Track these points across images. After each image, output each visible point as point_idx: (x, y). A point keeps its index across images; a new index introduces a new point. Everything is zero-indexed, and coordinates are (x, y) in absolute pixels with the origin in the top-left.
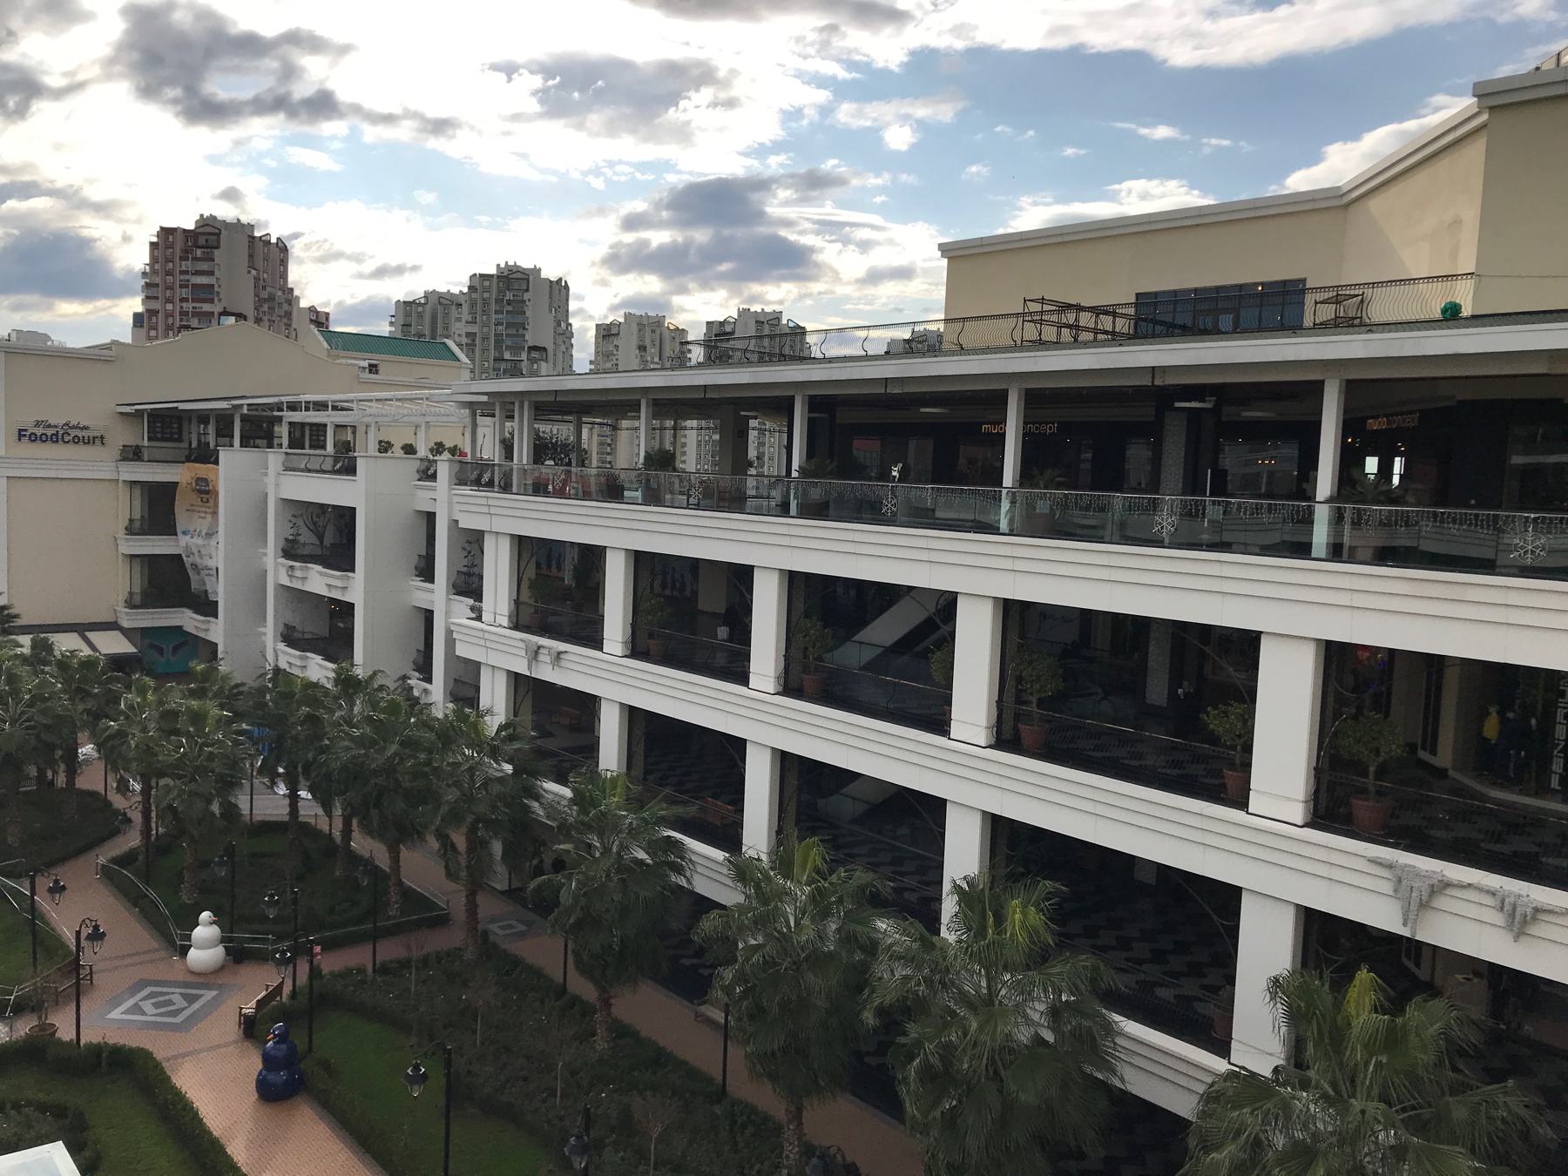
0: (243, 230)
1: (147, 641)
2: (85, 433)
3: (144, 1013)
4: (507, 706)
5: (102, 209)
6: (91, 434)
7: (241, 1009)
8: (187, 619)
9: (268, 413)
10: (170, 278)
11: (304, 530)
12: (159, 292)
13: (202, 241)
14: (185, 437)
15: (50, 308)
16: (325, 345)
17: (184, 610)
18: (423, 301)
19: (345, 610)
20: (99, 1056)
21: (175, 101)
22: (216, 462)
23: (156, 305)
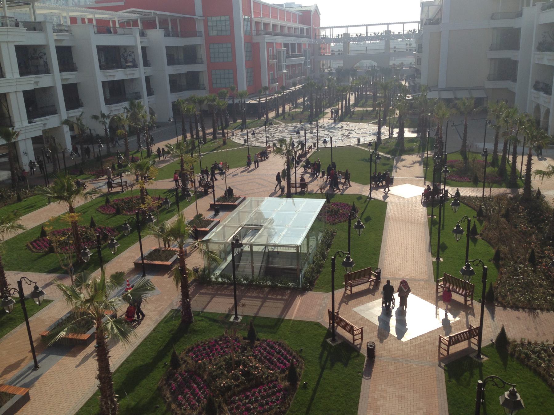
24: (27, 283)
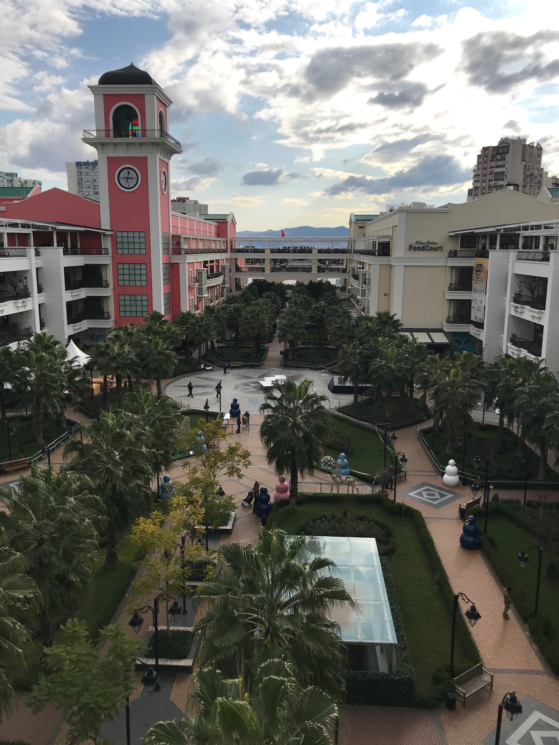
0: (521, 142)
1: (454, 338)
2: (435, 246)
3: (422, 496)
4: (187, 377)
5: (455, 143)
7: (460, 505)
8: (472, 330)
9: (514, 232)
10: (485, 171)
11: (524, 289)
12: (480, 178)
13: (501, 151)
15: (437, 190)
16: (550, 196)
17: (471, 325)
19: (540, 329)
20: (401, 509)
21: (486, 82)
22: (488, 257)
23: (478, 185)
24: (464, 600)
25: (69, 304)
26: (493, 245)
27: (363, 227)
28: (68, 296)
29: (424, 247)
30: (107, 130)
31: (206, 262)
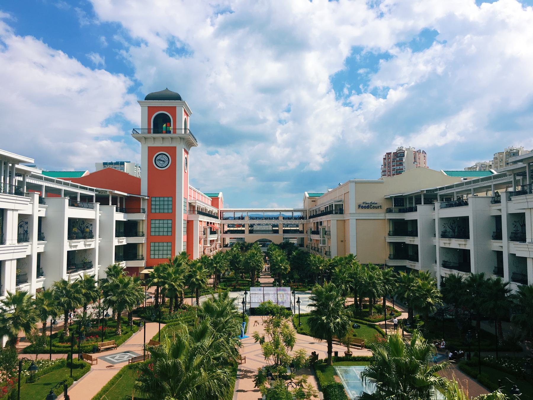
6: (378, 205)
13: (399, 155)
14: (405, 204)
18: (475, 167)
19: (466, 253)
25: (117, 247)
26: (418, 202)
27: (314, 201)
28: (116, 242)
29: (368, 206)
30: (149, 129)
31: (208, 223)
